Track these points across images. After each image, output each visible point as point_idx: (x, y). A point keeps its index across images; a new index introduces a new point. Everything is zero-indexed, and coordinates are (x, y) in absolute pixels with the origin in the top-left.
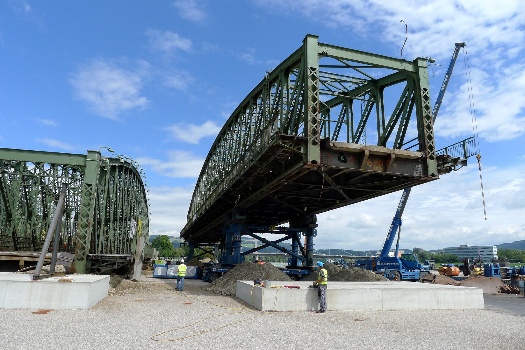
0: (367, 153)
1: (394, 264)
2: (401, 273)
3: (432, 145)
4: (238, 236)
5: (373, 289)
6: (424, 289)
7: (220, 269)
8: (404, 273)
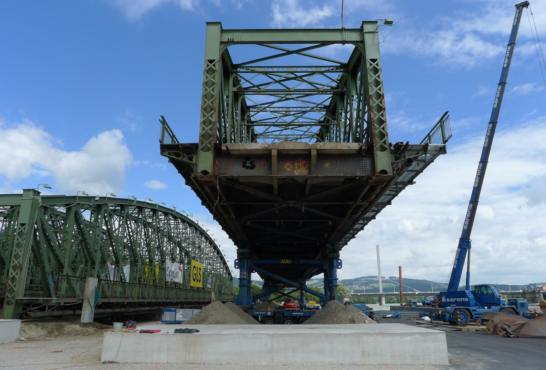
0: (274, 153)
1: (462, 300)
2: (472, 311)
3: (383, 132)
4: (243, 273)
5: (257, 334)
6: (340, 334)
7: (257, 313)
8: (475, 310)
